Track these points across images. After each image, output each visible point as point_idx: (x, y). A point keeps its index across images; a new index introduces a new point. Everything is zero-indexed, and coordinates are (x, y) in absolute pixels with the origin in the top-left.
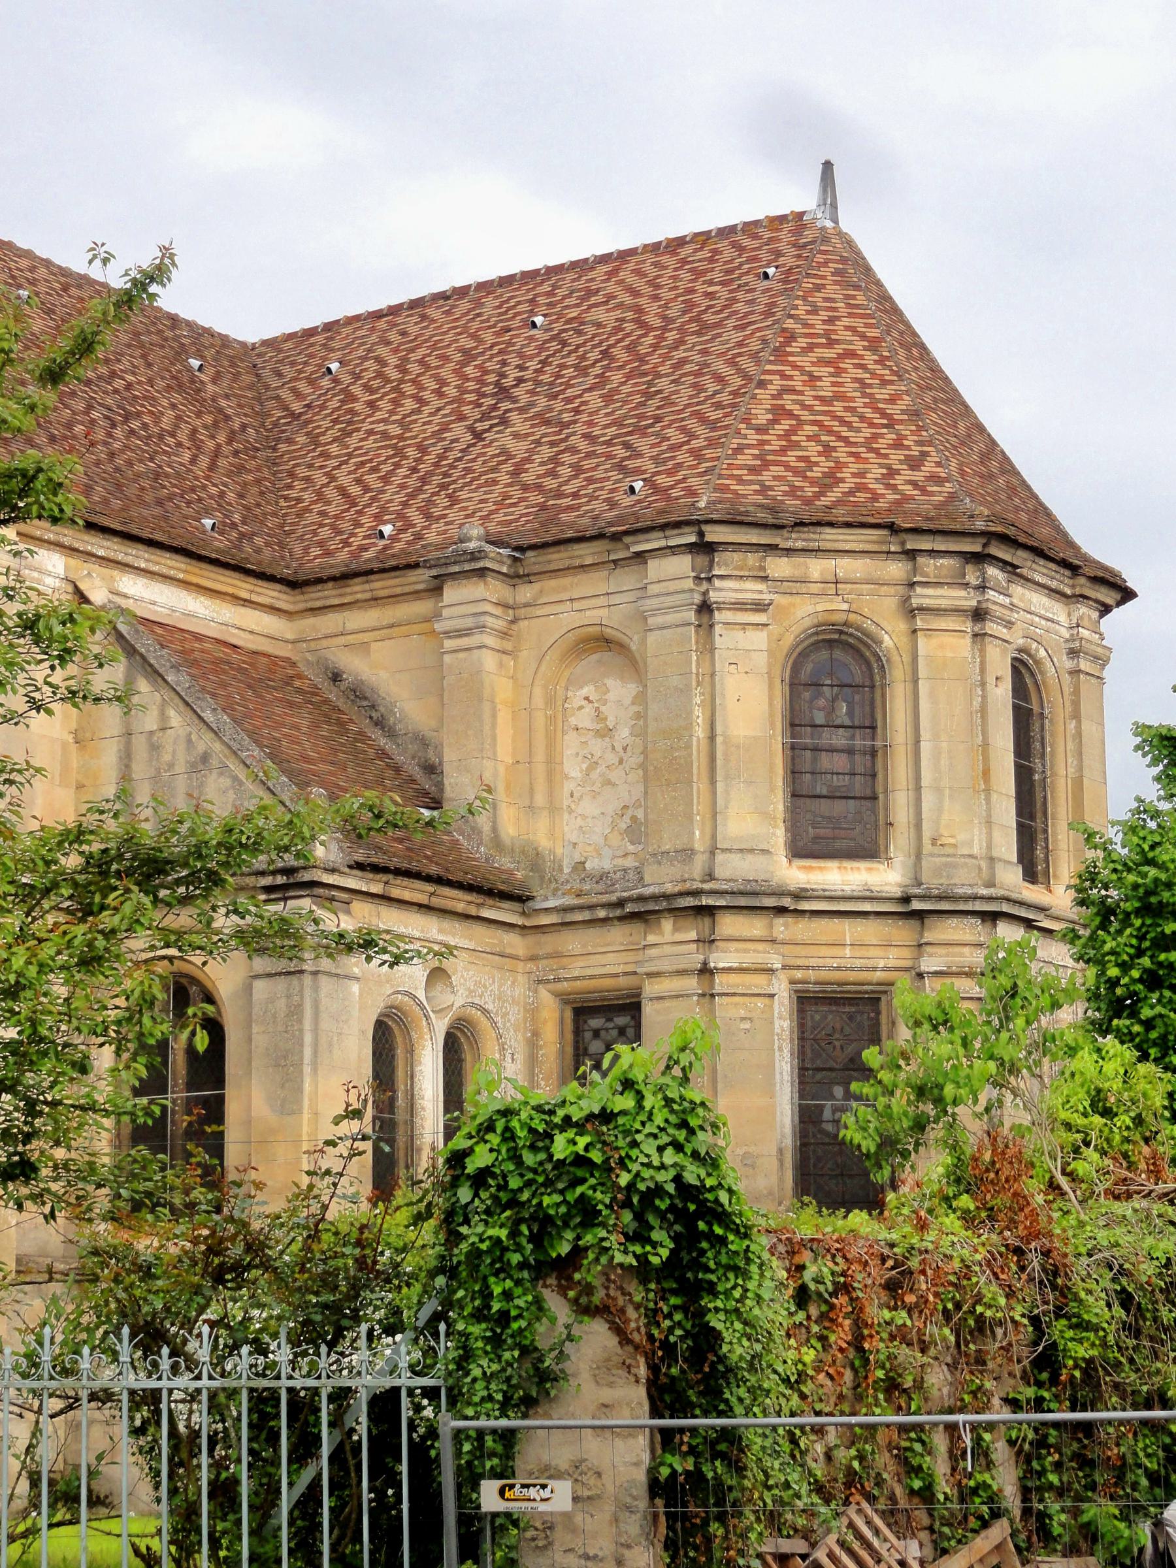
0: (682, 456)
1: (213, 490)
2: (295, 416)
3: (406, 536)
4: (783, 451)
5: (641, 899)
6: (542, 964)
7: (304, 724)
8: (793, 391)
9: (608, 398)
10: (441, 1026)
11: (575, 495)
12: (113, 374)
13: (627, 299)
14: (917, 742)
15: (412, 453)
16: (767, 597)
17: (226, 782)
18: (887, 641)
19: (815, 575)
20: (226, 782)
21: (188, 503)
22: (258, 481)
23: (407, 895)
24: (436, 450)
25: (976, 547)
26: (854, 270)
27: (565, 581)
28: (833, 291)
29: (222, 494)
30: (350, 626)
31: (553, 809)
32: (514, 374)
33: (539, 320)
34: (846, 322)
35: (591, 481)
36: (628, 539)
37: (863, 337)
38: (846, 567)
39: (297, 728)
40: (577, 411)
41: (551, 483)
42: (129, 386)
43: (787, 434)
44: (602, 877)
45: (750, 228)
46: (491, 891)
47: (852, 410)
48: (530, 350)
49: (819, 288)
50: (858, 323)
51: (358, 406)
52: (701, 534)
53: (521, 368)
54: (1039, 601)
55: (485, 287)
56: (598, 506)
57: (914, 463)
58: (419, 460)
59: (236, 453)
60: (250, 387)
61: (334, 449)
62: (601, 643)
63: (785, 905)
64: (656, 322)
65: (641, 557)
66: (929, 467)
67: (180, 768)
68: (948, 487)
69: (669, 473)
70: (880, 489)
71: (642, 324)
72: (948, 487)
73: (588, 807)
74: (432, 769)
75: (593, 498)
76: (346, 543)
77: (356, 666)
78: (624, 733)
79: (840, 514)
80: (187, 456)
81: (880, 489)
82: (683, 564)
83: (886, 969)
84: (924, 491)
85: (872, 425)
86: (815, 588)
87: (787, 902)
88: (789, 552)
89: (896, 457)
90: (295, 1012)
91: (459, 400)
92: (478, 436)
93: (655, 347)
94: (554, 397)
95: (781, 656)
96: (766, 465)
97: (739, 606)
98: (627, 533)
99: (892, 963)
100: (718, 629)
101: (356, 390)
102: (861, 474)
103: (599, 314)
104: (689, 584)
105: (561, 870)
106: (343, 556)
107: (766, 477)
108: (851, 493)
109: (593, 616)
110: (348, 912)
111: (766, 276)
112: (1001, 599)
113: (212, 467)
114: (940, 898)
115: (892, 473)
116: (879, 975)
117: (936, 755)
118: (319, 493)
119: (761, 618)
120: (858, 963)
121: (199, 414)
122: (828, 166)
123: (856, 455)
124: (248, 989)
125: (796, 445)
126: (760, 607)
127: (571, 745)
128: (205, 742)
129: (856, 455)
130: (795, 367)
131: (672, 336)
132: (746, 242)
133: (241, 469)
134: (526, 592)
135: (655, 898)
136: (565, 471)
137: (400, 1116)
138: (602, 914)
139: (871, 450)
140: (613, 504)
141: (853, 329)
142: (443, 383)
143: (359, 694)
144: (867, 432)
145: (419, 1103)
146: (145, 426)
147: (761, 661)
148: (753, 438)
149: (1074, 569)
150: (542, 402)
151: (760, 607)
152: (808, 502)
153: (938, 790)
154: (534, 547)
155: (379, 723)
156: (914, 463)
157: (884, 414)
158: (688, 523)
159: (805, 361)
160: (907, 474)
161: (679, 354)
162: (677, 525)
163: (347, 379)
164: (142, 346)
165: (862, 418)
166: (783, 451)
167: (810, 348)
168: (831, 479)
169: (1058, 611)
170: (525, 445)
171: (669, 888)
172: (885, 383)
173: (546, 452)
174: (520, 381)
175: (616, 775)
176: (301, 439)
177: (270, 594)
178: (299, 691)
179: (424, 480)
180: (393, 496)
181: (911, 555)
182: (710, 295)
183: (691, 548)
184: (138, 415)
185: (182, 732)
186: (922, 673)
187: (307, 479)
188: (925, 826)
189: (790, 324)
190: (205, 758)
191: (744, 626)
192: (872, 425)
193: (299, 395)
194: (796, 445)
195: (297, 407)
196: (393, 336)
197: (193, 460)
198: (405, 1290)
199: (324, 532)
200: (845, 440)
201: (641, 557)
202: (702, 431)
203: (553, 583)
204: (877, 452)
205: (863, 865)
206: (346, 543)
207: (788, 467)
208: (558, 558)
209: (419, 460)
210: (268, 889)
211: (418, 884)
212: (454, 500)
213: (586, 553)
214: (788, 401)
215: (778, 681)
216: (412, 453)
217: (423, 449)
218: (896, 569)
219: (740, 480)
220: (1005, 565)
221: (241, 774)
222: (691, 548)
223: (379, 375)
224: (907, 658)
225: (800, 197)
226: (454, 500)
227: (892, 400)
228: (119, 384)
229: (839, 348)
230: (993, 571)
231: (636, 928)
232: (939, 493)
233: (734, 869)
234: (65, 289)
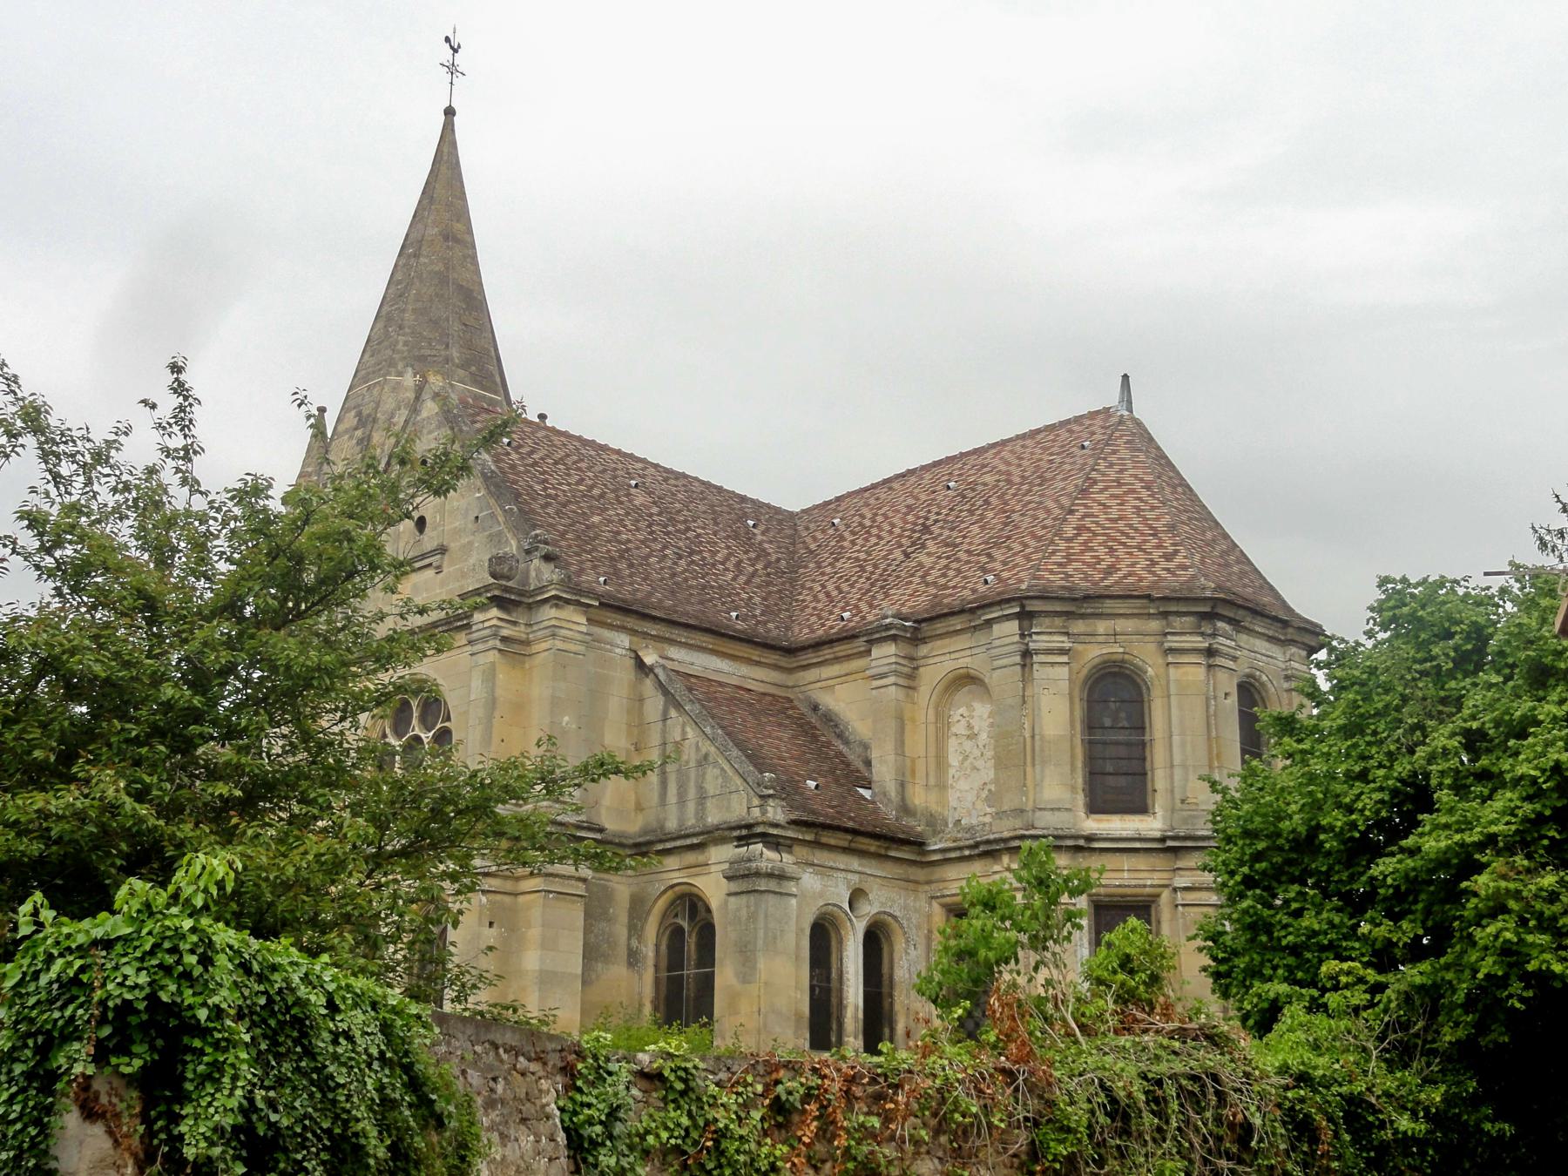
0: (1019, 560)
1: (745, 596)
2: (811, 552)
3: (857, 619)
4: (1082, 552)
5: (988, 842)
6: (933, 886)
7: (786, 736)
8: (1092, 515)
9: (983, 528)
10: (861, 926)
11: (954, 587)
12: (688, 529)
13: (1003, 467)
14: (1171, 736)
15: (869, 568)
16: (1067, 645)
17: (717, 771)
18: (1150, 671)
19: (1101, 630)
20: (717, 771)
21: (723, 603)
22: (780, 591)
23: (833, 842)
24: (882, 566)
25: (1207, 609)
26: (1143, 439)
27: (947, 641)
28: (1125, 453)
29: (751, 598)
30: (824, 676)
31: (942, 786)
32: (933, 517)
33: (951, 484)
34: (1131, 472)
35: (965, 578)
36: (979, 612)
37: (1142, 480)
38: (1121, 625)
39: (780, 739)
40: (964, 537)
41: (942, 581)
42: (699, 535)
43: (1086, 542)
44: (970, 829)
45: (1078, 420)
46: (895, 843)
47: (1131, 526)
48: (944, 503)
49: (1114, 452)
50: (1139, 472)
51: (846, 544)
52: (1023, 606)
53: (938, 514)
54: (1261, 645)
55: (924, 468)
56: (966, 593)
57: (1168, 557)
58: (872, 573)
59: (768, 575)
60: (789, 537)
61: (828, 570)
62: (966, 680)
63: (1084, 845)
64: (1017, 480)
65: (989, 623)
66: (1179, 559)
67: (692, 764)
68: (1191, 571)
69: (1009, 570)
70: (1144, 574)
71: (1009, 482)
72: (1191, 571)
73: (963, 785)
74: (868, 763)
75: (964, 588)
76: (823, 625)
77: (829, 701)
78: (984, 736)
79: (1116, 591)
80: (731, 575)
81: (1144, 574)
82: (1014, 626)
83: (1152, 886)
84: (1174, 574)
85: (1143, 534)
86: (1101, 639)
87: (1082, 842)
88: (1083, 616)
89: (1156, 554)
90: (752, 917)
91: (900, 536)
92: (907, 555)
93: (1015, 495)
94: (952, 529)
95: (1079, 683)
96: (1070, 561)
97: (1049, 652)
98: (978, 608)
99: (1156, 882)
100: (1036, 667)
101: (846, 534)
102: (1133, 565)
103: (988, 478)
104: (1017, 638)
105: (946, 825)
106: (821, 632)
107: (1069, 570)
108: (1125, 577)
109: (962, 663)
110: (790, 853)
111: (1083, 447)
112: (1228, 642)
113: (748, 582)
114: (1185, 838)
115: (1153, 563)
116: (1148, 890)
117: (1183, 745)
118: (815, 596)
119: (1065, 659)
120: (1133, 882)
121: (746, 552)
122: (1125, 377)
123: (1130, 554)
124: (726, 902)
125: (1091, 549)
126: (1062, 651)
127: (952, 743)
128: (707, 747)
129: (1130, 554)
130: (1094, 500)
131: (1025, 487)
132: (1076, 428)
133: (769, 584)
134: (923, 650)
135: (996, 841)
136: (951, 573)
137: (834, 984)
138: (967, 853)
139: (1140, 549)
140: (974, 591)
141: (1135, 476)
142: (893, 526)
143: (829, 719)
144: (1139, 539)
145: (845, 976)
146: (703, 559)
147: (1065, 686)
148: (1063, 545)
149: (1285, 624)
150: (946, 533)
151: (1062, 651)
152: (1096, 584)
153: (1184, 766)
154: (925, 620)
155: (840, 736)
156: (1168, 557)
157: (1151, 528)
158: (1013, 599)
159: (1101, 497)
160: (1164, 564)
161: (1028, 498)
162: (1008, 601)
163: (842, 528)
164: (714, 512)
165: (1136, 530)
166: (1082, 552)
167: (1106, 488)
168: (1112, 569)
169: (1276, 651)
170: (933, 559)
171: (1006, 835)
172: (1153, 508)
173: (944, 562)
174: (936, 521)
175: (980, 764)
176: (812, 565)
177: (773, 658)
178: (789, 717)
179: (873, 585)
180: (854, 596)
181: (1165, 615)
182: (1051, 462)
183: (1018, 616)
184: (701, 552)
185: (693, 741)
186: (1173, 690)
187: (811, 589)
188: (1176, 790)
189: (1094, 475)
190: (706, 756)
191: (1053, 664)
192: (1143, 534)
193: (815, 539)
194: (1091, 549)
195: (813, 547)
196: (872, 501)
197: (734, 579)
198: (1086, 1106)
199: (814, 619)
200: (1124, 544)
201: (989, 623)
202: (1033, 543)
203: (939, 643)
204: (1144, 551)
205: (1137, 818)
206: (823, 625)
207: (1084, 563)
208: (940, 627)
209: (872, 573)
210: (739, 838)
211: (840, 835)
212: (887, 595)
213: (957, 623)
214: (1088, 522)
215: (1077, 700)
216: (869, 568)
217: (876, 566)
218: (1155, 625)
219: (1051, 572)
220: (1230, 621)
221: (727, 767)
222: (1018, 616)
223: (860, 524)
224: (1163, 682)
225: (1112, 398)
226: (887, 595)
227: (1157, 519)
228: (691, 534)
229: (1125, 489)
230: (1220, 624)
231: (989, 861)
232: (1184, 576)
233: (1049, 821)
234: (666, 480)
